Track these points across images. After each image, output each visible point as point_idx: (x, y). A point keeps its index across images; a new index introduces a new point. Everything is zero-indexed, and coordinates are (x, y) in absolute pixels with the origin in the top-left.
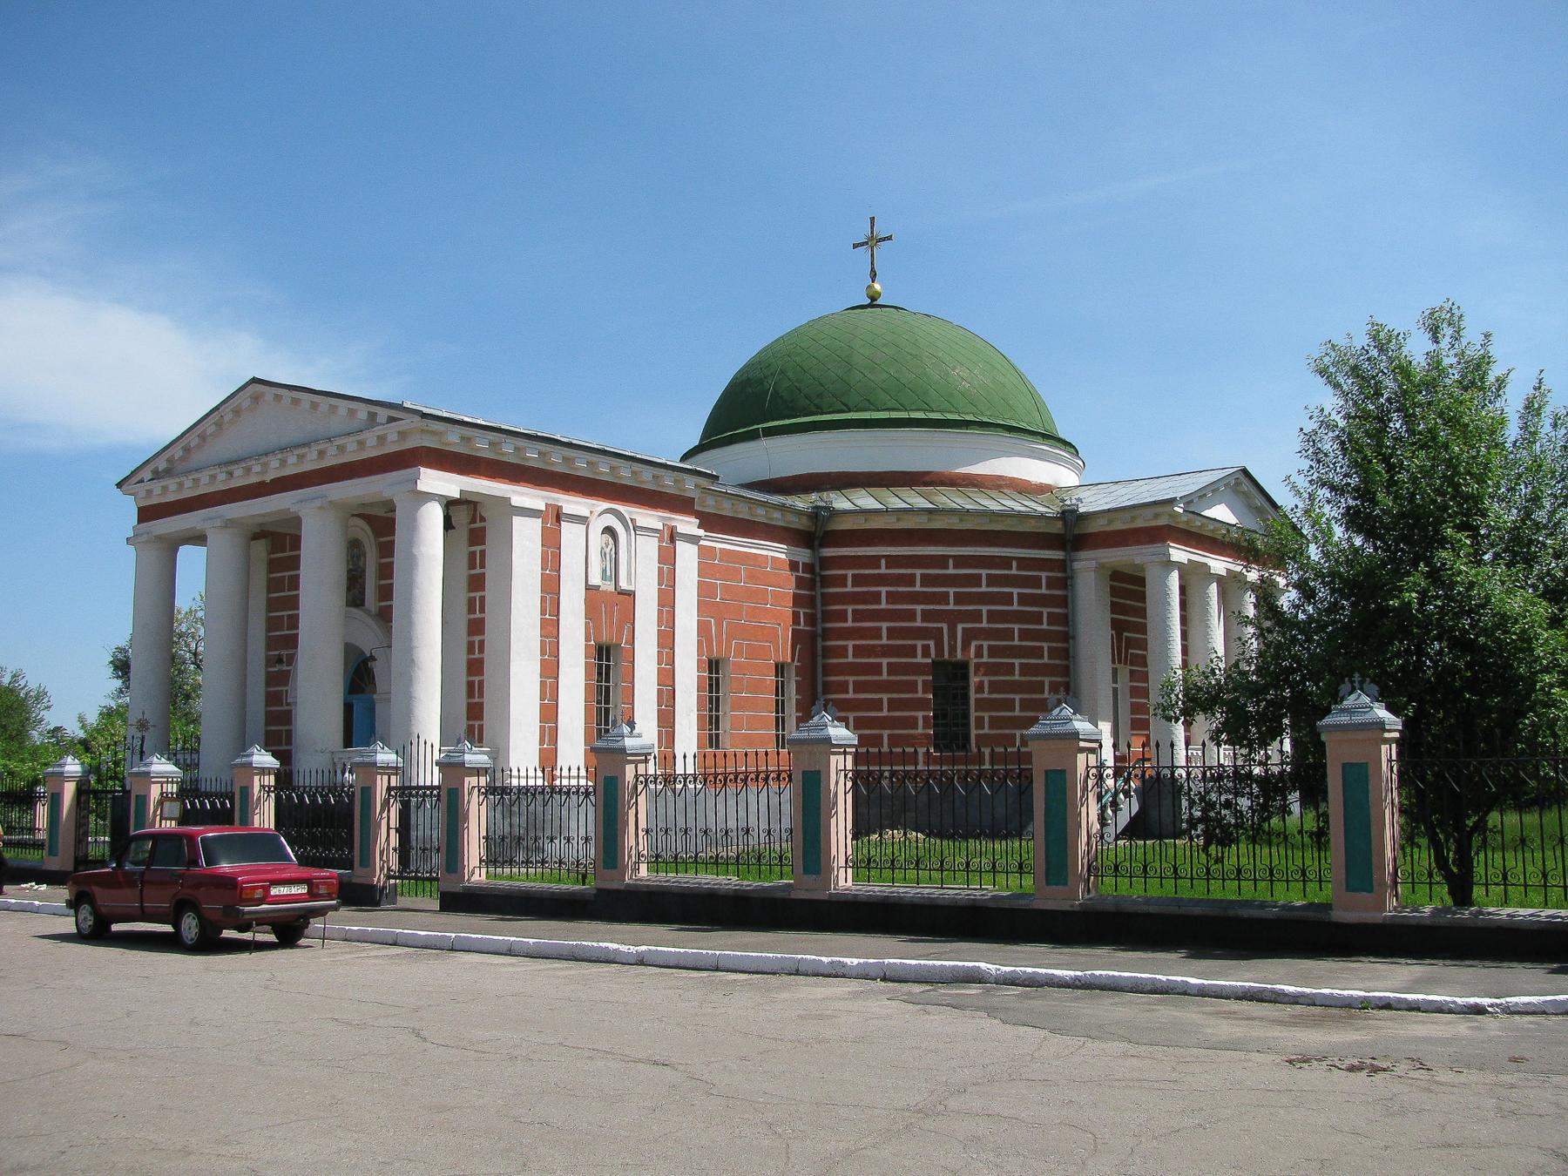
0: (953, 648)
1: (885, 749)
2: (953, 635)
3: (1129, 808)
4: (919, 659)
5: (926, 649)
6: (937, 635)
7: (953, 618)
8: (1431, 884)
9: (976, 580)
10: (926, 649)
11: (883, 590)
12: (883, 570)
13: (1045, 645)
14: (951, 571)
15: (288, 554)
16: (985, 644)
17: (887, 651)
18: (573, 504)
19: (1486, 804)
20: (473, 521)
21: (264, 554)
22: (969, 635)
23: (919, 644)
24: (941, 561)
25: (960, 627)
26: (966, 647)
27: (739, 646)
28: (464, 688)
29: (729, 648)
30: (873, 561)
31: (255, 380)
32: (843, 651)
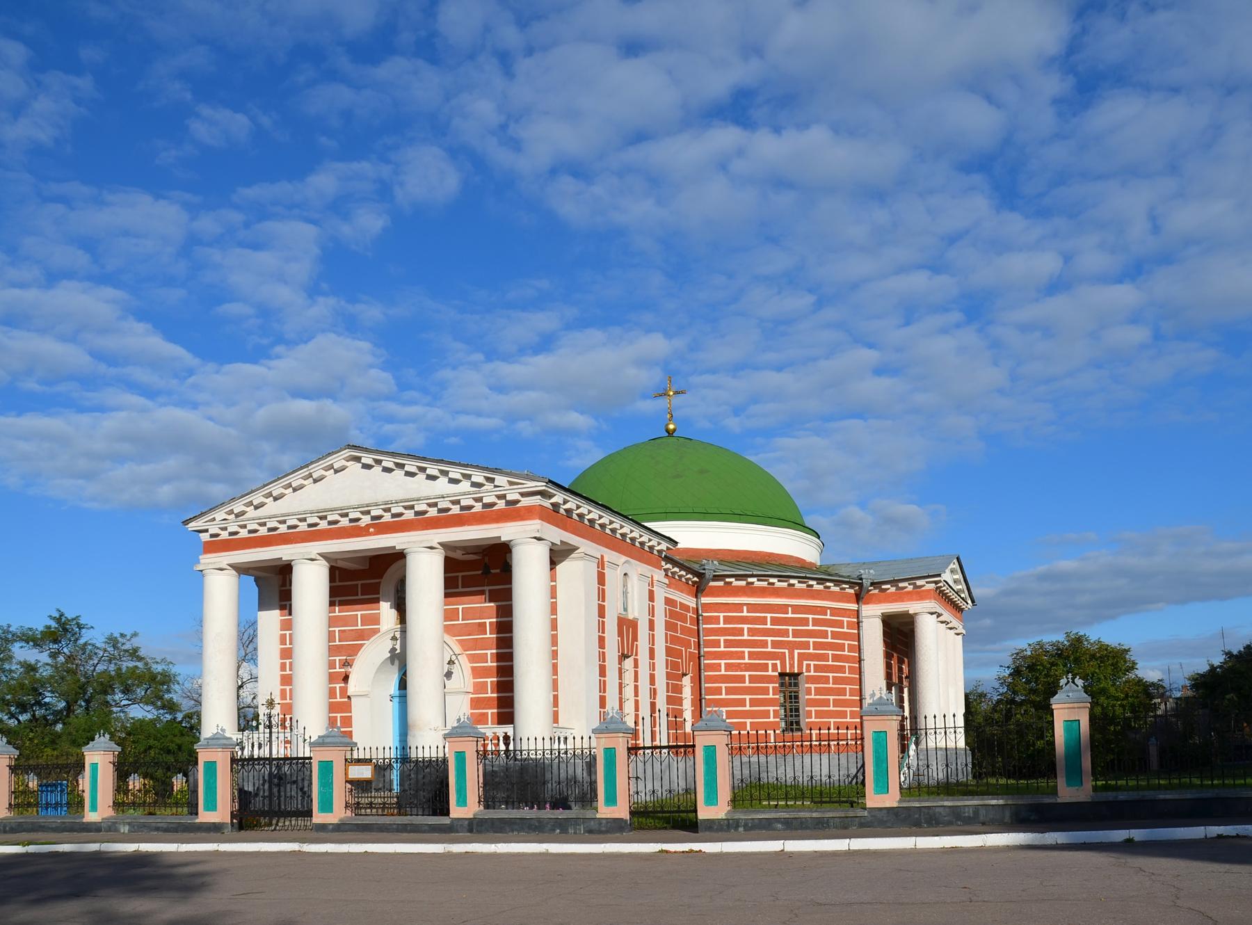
0: (792, 666)
2: (792, 658)
4: (770, 673)
5: (774, 666)
6: (782, 657)
7: (792, 646)
9: (805, 622)
10: (774, 666)
11: (746, 627)
12: (745, 614)
14: (790, 615)
16: (812, 663)
17: (749, 667)
18: (610, 556)
22: (802, 657)
23: (770, 662)
24: (783, 609)
26: (800, 665)
27: (808, 665)
29: (800, 665)
30: (738, 607)
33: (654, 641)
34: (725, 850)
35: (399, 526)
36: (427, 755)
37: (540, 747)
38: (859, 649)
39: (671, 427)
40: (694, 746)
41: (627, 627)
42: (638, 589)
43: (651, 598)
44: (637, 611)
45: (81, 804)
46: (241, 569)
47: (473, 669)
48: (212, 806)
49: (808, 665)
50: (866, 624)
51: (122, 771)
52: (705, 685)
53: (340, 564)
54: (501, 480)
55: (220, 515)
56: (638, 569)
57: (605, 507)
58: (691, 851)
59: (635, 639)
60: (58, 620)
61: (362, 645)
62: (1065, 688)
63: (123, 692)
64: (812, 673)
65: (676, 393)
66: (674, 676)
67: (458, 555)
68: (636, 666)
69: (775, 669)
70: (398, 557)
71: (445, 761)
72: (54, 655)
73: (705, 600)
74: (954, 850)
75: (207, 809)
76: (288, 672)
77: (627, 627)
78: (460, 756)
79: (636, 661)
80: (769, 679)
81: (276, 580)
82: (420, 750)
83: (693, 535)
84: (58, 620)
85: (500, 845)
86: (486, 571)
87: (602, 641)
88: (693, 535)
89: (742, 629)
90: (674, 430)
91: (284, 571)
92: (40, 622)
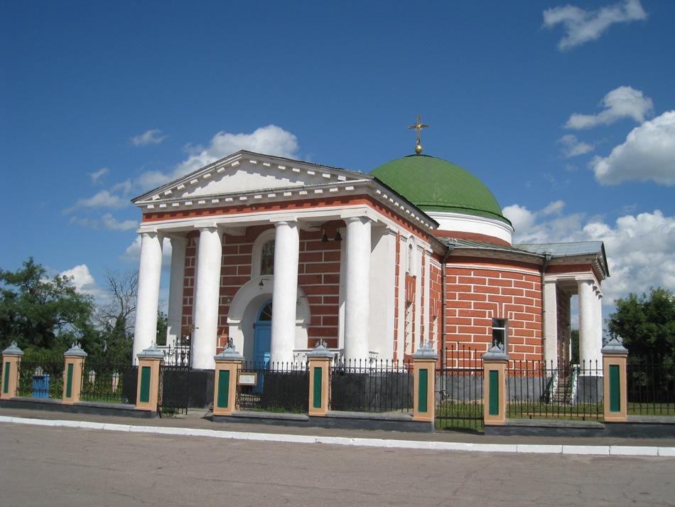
0: (501, 313)
1: (472, 352)
2: (501, 308)
3: (43, 349)
5: (490, 313)
6: (494, 307)
7: (501, 300)
8: (641, 409)
10: (490, 313)
13: (535, 315)
15: (305, 263)
16: (513, 312)
17: (474, 314)
18: (392, 225)
19: (269, 370)
20: (189, 245)
21: (183, 266)
22: (508, 308)
25: (504, 304)
26: (506, 314)
27: (511, 314)
28: (180, 319)
29: (506, 314)
31: (243, 152)
32: (453, 313)
33: (424, 292)
34: (250, 438)
35: (269, 206)
36: (280, 368)
37: (363, 366)
38: (542, 304)
39: (419, 147)
40: (482, 370)
41: (410, 280)
42: (416, 257)
43: (423, 264)
44: (416, 272)
45: (61, 393)
46: (162, 234)
47: (311, 307)
48: (145, 398)
49: (511, 314)
50: (547, 287)
51: (87, 367)
52: (446, 325)
53: (229, 232)
54: (342, 178)
55: (155, 197)
56: (419, 241)
57: (403, 198)
58: (79, 428)
59: (414, 291)
60: (28, 265)
61: (239, 288)
62: (227, 350)
63: (61, 315)
64: (513, 319)
65: (422, 126)
66: (433, 318)
67: (307, 229)
68: (414, 311)
69: (490, 316)
70: (272, 226)
71: (307, 372)
72: (23, 289)
73: (449, 265)
74: (409, 451)
75: (142, 400)
76: (188, 305)
77: (410, 280)
78: (318, 371)
79: (414, 306)
80: (486, 323)
81: (184, 241)
82: (280, 365)
83: (449, 223)
84: (28, 265)
85: (356, 439)
86: (325, 239)
87: (397, 290)
88: (449, 223)
89: (470, 287)
90: (421, 151)
91: (194, 234)
92: (17, 267)
